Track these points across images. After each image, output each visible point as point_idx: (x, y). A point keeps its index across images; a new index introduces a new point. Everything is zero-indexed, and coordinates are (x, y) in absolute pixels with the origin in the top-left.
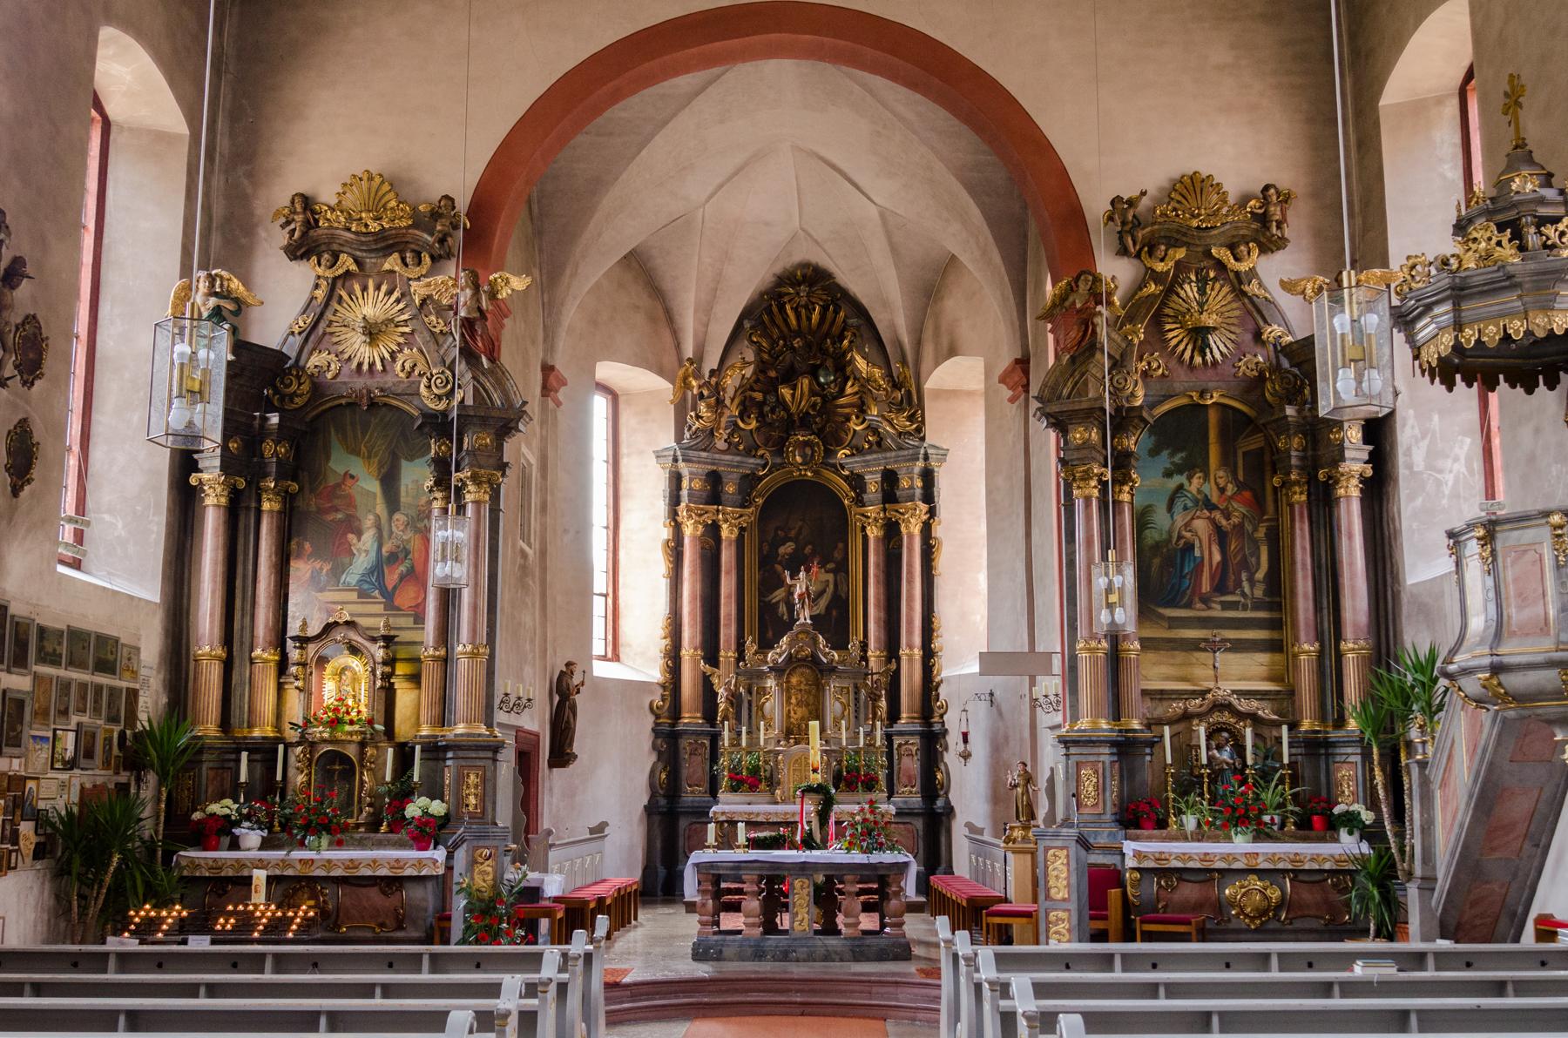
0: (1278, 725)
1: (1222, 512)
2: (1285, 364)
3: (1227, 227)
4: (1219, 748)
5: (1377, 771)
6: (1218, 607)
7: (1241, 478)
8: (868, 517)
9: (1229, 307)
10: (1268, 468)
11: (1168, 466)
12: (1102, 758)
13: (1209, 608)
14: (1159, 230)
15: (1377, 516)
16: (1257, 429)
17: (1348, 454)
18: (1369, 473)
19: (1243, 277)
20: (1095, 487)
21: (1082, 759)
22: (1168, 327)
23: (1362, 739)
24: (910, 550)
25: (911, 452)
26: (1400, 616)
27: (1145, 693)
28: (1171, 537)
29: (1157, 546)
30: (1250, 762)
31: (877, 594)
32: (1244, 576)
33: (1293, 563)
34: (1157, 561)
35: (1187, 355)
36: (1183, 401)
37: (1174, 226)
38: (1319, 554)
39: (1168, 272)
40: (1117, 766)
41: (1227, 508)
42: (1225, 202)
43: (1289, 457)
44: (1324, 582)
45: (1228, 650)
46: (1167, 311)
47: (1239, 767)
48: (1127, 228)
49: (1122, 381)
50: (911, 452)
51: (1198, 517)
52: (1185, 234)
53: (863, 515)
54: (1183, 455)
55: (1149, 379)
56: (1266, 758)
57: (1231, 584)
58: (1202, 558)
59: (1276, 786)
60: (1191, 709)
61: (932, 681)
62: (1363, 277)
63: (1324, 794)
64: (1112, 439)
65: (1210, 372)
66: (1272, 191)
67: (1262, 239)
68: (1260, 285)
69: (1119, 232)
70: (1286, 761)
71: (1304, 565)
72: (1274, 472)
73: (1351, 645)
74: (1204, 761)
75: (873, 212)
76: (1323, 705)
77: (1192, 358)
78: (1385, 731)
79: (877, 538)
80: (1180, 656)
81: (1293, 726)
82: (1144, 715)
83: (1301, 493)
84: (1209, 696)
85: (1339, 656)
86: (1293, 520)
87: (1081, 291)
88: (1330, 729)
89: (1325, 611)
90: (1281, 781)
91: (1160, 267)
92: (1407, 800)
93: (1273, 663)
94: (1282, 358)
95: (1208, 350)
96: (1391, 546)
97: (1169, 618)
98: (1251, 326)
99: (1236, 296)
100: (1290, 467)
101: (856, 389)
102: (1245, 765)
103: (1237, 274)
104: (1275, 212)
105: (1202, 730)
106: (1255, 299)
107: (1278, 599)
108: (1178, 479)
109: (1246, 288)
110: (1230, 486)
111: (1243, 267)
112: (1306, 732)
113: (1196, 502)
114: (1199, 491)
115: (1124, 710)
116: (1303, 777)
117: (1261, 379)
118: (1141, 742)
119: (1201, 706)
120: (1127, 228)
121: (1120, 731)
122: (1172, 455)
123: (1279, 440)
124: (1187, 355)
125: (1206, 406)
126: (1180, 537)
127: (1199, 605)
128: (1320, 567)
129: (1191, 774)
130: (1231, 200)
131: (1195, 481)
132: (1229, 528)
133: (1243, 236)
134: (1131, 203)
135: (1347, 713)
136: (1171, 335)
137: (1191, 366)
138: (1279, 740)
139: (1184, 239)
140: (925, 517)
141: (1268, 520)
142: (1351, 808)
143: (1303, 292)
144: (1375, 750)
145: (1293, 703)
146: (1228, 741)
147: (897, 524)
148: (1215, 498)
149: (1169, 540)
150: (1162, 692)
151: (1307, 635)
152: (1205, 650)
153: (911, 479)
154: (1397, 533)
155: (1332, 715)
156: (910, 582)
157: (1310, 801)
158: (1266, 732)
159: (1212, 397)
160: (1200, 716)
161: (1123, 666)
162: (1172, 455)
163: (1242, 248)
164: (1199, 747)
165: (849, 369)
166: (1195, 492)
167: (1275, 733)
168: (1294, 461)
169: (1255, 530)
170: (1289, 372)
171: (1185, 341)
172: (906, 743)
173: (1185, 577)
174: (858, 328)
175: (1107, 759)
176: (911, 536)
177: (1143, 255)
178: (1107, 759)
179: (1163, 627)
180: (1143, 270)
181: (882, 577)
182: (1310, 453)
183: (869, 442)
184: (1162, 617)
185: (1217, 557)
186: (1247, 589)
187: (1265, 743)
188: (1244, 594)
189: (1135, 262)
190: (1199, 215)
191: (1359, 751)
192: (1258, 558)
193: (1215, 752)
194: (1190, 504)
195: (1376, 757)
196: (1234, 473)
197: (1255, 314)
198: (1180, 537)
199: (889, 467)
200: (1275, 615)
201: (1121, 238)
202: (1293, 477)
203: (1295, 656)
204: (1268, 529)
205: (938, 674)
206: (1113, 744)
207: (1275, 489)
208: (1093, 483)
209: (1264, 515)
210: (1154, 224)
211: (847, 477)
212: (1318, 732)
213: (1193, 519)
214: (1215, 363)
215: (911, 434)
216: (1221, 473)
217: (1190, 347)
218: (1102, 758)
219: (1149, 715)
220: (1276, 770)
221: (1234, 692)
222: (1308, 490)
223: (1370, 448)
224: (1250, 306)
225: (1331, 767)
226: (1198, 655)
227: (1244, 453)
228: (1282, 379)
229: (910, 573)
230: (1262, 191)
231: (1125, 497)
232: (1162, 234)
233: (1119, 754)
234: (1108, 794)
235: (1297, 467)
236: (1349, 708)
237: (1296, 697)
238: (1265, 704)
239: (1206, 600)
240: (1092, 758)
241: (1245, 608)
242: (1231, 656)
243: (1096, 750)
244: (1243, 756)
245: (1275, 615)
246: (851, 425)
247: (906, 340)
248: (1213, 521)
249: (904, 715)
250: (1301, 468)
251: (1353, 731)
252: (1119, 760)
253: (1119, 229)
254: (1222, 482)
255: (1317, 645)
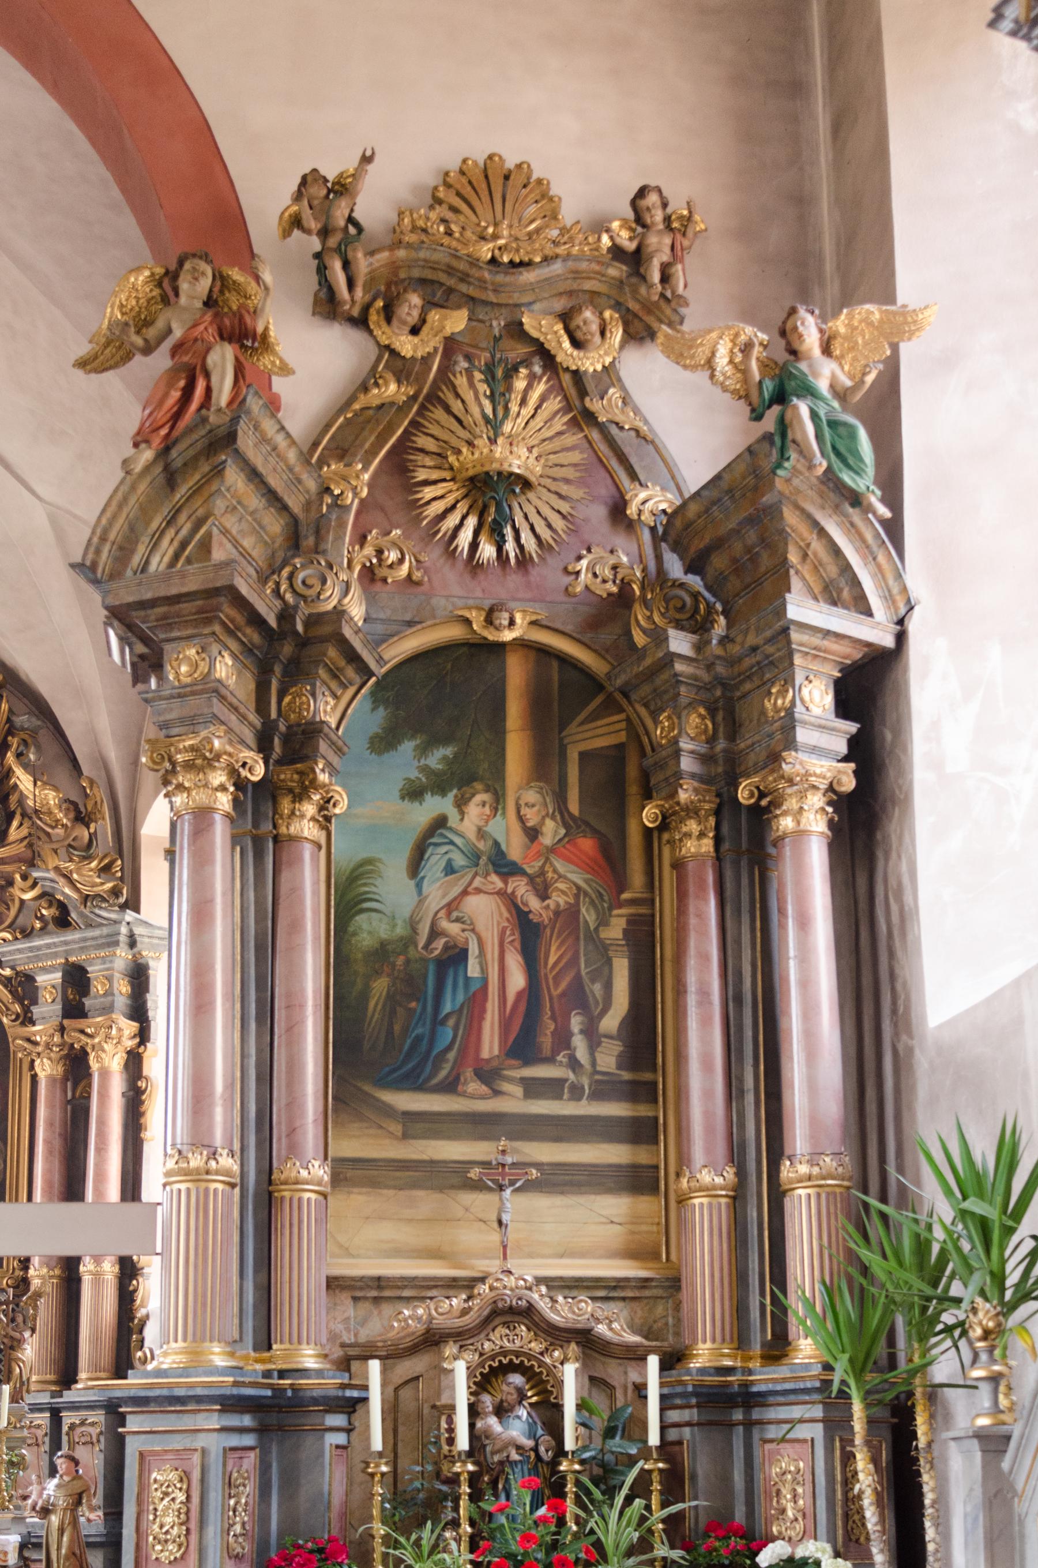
0: (637, 1356)
1: (531, 879)
2: (675, 567)
3: (557, 267)
4: (501, 1411)
5: (862, 1463)
6: (518, 1091)
7: (574, 807)
8: (36, 1044)
9: (556, 444)
10: (633, 789)
11: (414, 774)
12: (201, 1441)
13: (497, 1093)
14: (410, 264)
15: (863, 905)
16: (610, 706)
17: (802, 735)
18: (849, 784)
19: (590, 385)
20: (223, 788)
21: (155, 1445)
22: (422, 475)
23: (827, 1383)
24: (104, 1096)
25: (105, 931)
26: (911, 1108)
27: (334, 1284)
28: (414, 931)
29: (382, 953)
30: (569, 1445)
31: (47, 1172)
32: (576, 1023)
33: (680, 990)
34: (380, 986)
35: (466, 536)
36: (454, 632)
37: (440, 256)
38: (739, 974)
39: (427, 360)
40: (251, 1459)
41: (542, 873)
42: (555, 217)
43: (677, 753)
44: (748, 1033)
45: (530, 1186)
46: (422, 441)
47: (547, 1456)
48: (333, 242)
49: (315, 581)
50: (105, 931)
51: (478, 891)
52: (464, 278)
53: (29, 1040)
54: (448, 751)
55: (378, 586)
56: (609, 1433)
57: (546, 1041)
58: (485, 981)
59: (629, 1501)
60: (439, 1322)
61: (132, 1319)
62: (840, 325)
63: (740, 1516)
64: (281, 694)
65: (514, 580)
66: (653, 198)
67: (633, 305)
68: (626, 400)
69: (318, 256)
70: (654, 1439)
71: (704, 994)
72: (647, 795)
73: (803, 1169)
74: (463, 1442)
75: (40, 517)
76: (741, 1311)
77: (474, 546)
78: (877, 1368)
79: (52, 1079)
80: (427, 1201)
81: (672, 1361)
82: (333, 1337)
83: (702, 835)
84: (483, 1289)
85: (778, 1196)
86: (682, 895)
87: (183, 300)
88: (755, 1364)
89: (750, 1098)
90: (641, 1488)
91: (407, 346)
92: (930, 1533)
93: (635, 1220)
94: (683, 701)
95: (508, 531)
96: (891, 954)
97: (406, 1114)
98: (605, 490)
99: (574, 423)
100: (678, 775)
101: (24, 831)
102: (560, 1452)
103: (577, 375)
104: (659, 245)
105: (460, 1370)
106: (614, 430)
107: (647, 1076)
108: (435, 805)
109: (594, 404)
110: (550, 825)
111: (590, 363)
112: (702, 1371)
113: (474, 857)
114: (481, 833)
115: (282, 1324)
116: (693, 1477)
117: (623, 599)
118: (315, 1401)
119: (465, 1312)
120: (333, 242)
121: (267, 1374)
122: (423, 750)
123: (656, 722)
124: (466, 536)
125: (500, 647)
126: (435, 933)
127: (474, 1086)
128: (739, 1000)
129: (438, 1474)
130: (568, 214)
131: (474, 810)
132: (546, 917)
133: (594, 294)
134: (342, 188)
135: (792, 1321)
136: (428, 492)
137: (473, 565)
138: (640, 1391)
139: (463, 288)
140: (130, 1044)
141: (632, 902)
142: (800, 1552)
143: (709, 363)
144: (858, 1409)
145: (678, 1307)
146: (522, 1396)
147: (83, 1054)
148: (515, 849)
149: (409, 941)
150: (379, 1282)
151: (709, 1150)
152: (478, 1186)
153: (109, 979)
154: (907, 918)
155: (759, 1335)
156: (101, 1149)
157: (706, 1535)
158: (614, 1372)
159: (512, 623)
160: (461, 1337)
161: (283, 1218)
162: (423, 750)
163: (588, 314)
164: (452, 1408)
165: (13, 799)
166: (471, 835)
167: (634, 1376)
168: (686, 764)
169: (603, 922)
170: (682, 585)
171: (462, 508)
172: (83, 1423)
173: (443, 1022)
174: (34, 733)
175: (215, 1444)
176: (105, 1073)
177: (373, 317)
178: (215, 1444)
179: (391, 1135)
180: (373, 352)
181: (57, 1143)
182: (721, 745)
183: (41, 918)
184: (388, 1111)
185: (517, 980)
186: (581, 1053)
187: (612, 1397)
188: (574, 1064)
189: (357, 335)
190: (495, 237)
191: (818, 1412)
192: (608, 986)
193: (493, 1421)
194: (459, 860)
195: (858, 1426)
196: (561, 798)
197: (614, 464)
198: (435, 933)
199: (72, 959)
200: (643, 1111)
201: (322, 270)
202: (683, 796)
203: (683, 1200)
204: (632, 921)
205: (142, 1306)
206: (230, 1404)
207: (648, 832)
208: (218, 778)
209: (622, 891)
210: (398, 244)
211: (9, 979)
212: (729, 1371)
213: (465, 893)
214: (524, 560)
215: (104, 900)
216: (531, 796)
217: (472, 522)
218: (201, 1441)
219: (348, 1338)
220: (632, 1461)
221: (539, 1280)
222: (718, 827)
223: (852, 727)
224: (602, 448)
225: (757, 1452)
226: (469, 1198)
227: (583, 755)
228: (667, 600)
229: (102, 1135)
230: (634, 203)
231: (307, 828)
232: (416, 273)
233: (262, 1430)
234: (212, 1531)
235: (693, 776)
236: (796, 1305)
237: (684, 1295)
238: (613, 1308)
239: (489, 1075)
240: (177, 1443)
241: (576, 1092)
242: (541, 1203)
243: (187, 1422)
244: (556, 1430)
245: (643, 1111)
246: (16, 891)
247: (114, 756)
248: (510, 900)
249: (82, 1375)
250: (705, 780)
251: (807, 1366)
252: (264, 1448)
253: (316, 244)
254: (532, 817)
255: (730, 1173)
